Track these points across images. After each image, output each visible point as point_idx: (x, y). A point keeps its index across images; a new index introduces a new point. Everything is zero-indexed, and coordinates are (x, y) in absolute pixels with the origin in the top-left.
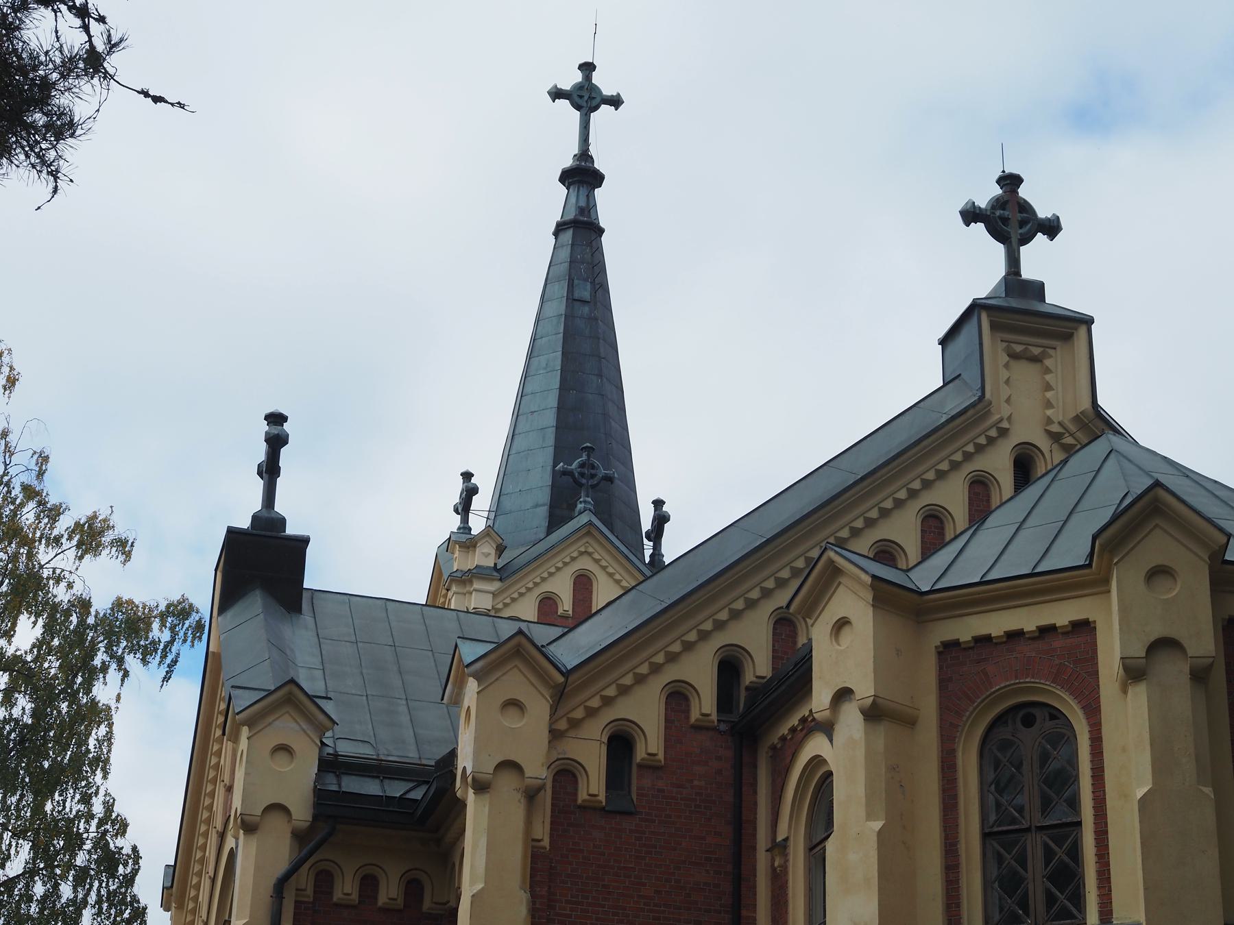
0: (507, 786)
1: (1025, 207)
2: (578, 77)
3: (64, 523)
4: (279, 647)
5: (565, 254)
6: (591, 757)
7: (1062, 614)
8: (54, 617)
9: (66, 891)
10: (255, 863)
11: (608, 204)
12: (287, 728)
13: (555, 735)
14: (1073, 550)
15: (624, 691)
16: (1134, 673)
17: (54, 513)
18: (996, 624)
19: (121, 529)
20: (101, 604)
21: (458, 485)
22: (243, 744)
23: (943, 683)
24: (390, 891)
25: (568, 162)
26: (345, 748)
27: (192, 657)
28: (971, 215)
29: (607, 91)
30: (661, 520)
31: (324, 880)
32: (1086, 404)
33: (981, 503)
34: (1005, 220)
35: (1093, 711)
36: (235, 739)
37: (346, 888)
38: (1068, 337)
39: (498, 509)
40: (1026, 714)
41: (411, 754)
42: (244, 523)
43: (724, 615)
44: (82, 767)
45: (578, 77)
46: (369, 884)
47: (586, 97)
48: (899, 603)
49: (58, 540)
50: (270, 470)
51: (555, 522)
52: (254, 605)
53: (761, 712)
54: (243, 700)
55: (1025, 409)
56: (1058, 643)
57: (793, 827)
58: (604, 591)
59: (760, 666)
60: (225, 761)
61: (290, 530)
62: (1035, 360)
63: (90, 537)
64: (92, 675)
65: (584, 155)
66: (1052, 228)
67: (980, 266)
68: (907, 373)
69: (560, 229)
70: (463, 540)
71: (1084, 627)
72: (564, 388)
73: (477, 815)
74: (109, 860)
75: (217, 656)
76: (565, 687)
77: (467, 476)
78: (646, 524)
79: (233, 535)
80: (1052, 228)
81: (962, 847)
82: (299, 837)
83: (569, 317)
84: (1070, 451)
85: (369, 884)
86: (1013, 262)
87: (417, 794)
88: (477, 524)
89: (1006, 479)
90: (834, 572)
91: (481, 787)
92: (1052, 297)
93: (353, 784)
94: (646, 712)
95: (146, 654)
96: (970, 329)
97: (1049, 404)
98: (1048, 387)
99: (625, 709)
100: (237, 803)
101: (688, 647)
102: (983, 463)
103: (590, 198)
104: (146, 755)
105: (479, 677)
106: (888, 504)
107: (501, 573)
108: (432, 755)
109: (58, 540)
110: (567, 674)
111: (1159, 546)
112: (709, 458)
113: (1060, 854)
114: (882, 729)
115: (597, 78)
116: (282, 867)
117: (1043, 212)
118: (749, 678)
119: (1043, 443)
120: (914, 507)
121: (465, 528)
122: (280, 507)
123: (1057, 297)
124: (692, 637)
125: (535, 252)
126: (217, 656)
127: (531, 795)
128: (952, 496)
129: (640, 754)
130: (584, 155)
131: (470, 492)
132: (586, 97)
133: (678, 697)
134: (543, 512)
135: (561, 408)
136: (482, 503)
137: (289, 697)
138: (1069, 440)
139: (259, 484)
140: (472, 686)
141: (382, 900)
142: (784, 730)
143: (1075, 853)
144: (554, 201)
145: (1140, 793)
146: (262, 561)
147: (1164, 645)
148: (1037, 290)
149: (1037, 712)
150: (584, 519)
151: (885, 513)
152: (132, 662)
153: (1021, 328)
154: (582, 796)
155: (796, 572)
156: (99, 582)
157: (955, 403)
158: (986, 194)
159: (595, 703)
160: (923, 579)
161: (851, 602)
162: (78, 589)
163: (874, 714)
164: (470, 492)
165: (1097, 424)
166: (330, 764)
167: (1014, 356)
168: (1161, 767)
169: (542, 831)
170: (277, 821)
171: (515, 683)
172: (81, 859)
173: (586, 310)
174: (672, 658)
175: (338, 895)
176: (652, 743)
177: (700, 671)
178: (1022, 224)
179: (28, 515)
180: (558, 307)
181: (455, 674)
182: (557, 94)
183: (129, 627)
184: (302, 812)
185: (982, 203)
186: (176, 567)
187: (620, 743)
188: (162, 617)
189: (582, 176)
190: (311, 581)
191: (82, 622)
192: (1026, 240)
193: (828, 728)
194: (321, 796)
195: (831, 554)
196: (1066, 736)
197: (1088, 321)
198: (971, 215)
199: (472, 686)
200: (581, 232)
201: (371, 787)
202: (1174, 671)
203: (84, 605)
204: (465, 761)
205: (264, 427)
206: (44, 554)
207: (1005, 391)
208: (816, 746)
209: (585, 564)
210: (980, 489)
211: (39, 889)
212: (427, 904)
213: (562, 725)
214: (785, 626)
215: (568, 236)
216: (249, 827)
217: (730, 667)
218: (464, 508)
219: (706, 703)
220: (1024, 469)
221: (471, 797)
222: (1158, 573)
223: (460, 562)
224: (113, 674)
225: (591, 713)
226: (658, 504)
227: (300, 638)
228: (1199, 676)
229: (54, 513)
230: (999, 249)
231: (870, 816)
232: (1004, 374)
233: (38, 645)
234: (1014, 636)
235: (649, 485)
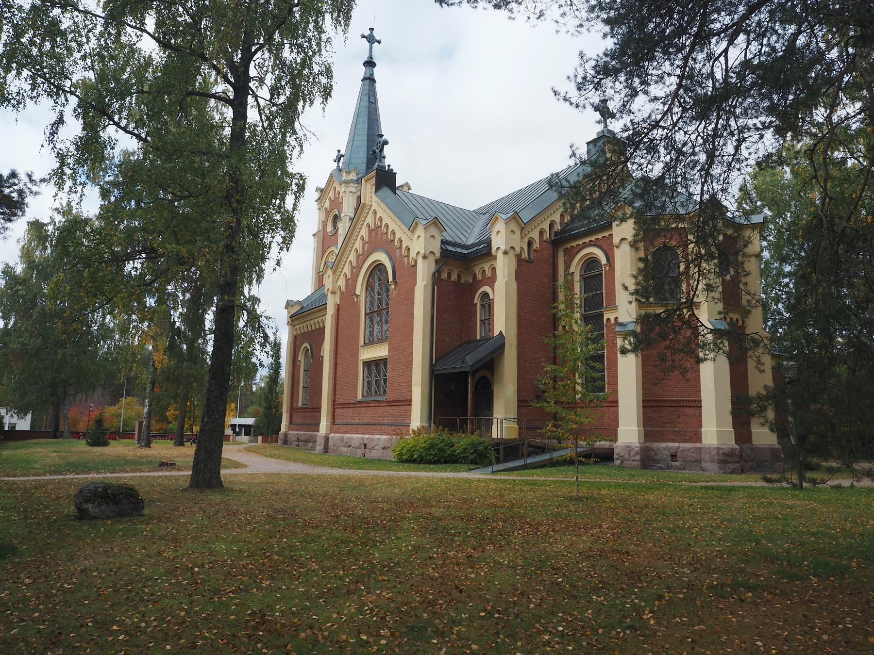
2: (369, 32)
11: (377, 72)
24: (454, 277)
29: (377, 38)
37: (444, 276)
40: (666, 248)
45: (369, 32)
46: (449, 274)
47: (371, 39)
65: (371, 57)
69: (364, 80)
72: (369, 129)
82: (437, 261)
83: (369, 107)
85: (449, 274)
99: (531, 235)
115: (374, 33)
121: (338, 166)
132: (371, 39)
133: (541, 233)
134: (365, 165)
135: (368, 135)
141: (453, 279)
142: (574, 244)
144: (362, 71)
166: (443, 242)
175: (443, 277)
177: (546, 226)
182: (363, 36)
184: (438, 255)
189: (370, 64)
200: (370, 80)
201: (459, 250)
212: (462, 281)
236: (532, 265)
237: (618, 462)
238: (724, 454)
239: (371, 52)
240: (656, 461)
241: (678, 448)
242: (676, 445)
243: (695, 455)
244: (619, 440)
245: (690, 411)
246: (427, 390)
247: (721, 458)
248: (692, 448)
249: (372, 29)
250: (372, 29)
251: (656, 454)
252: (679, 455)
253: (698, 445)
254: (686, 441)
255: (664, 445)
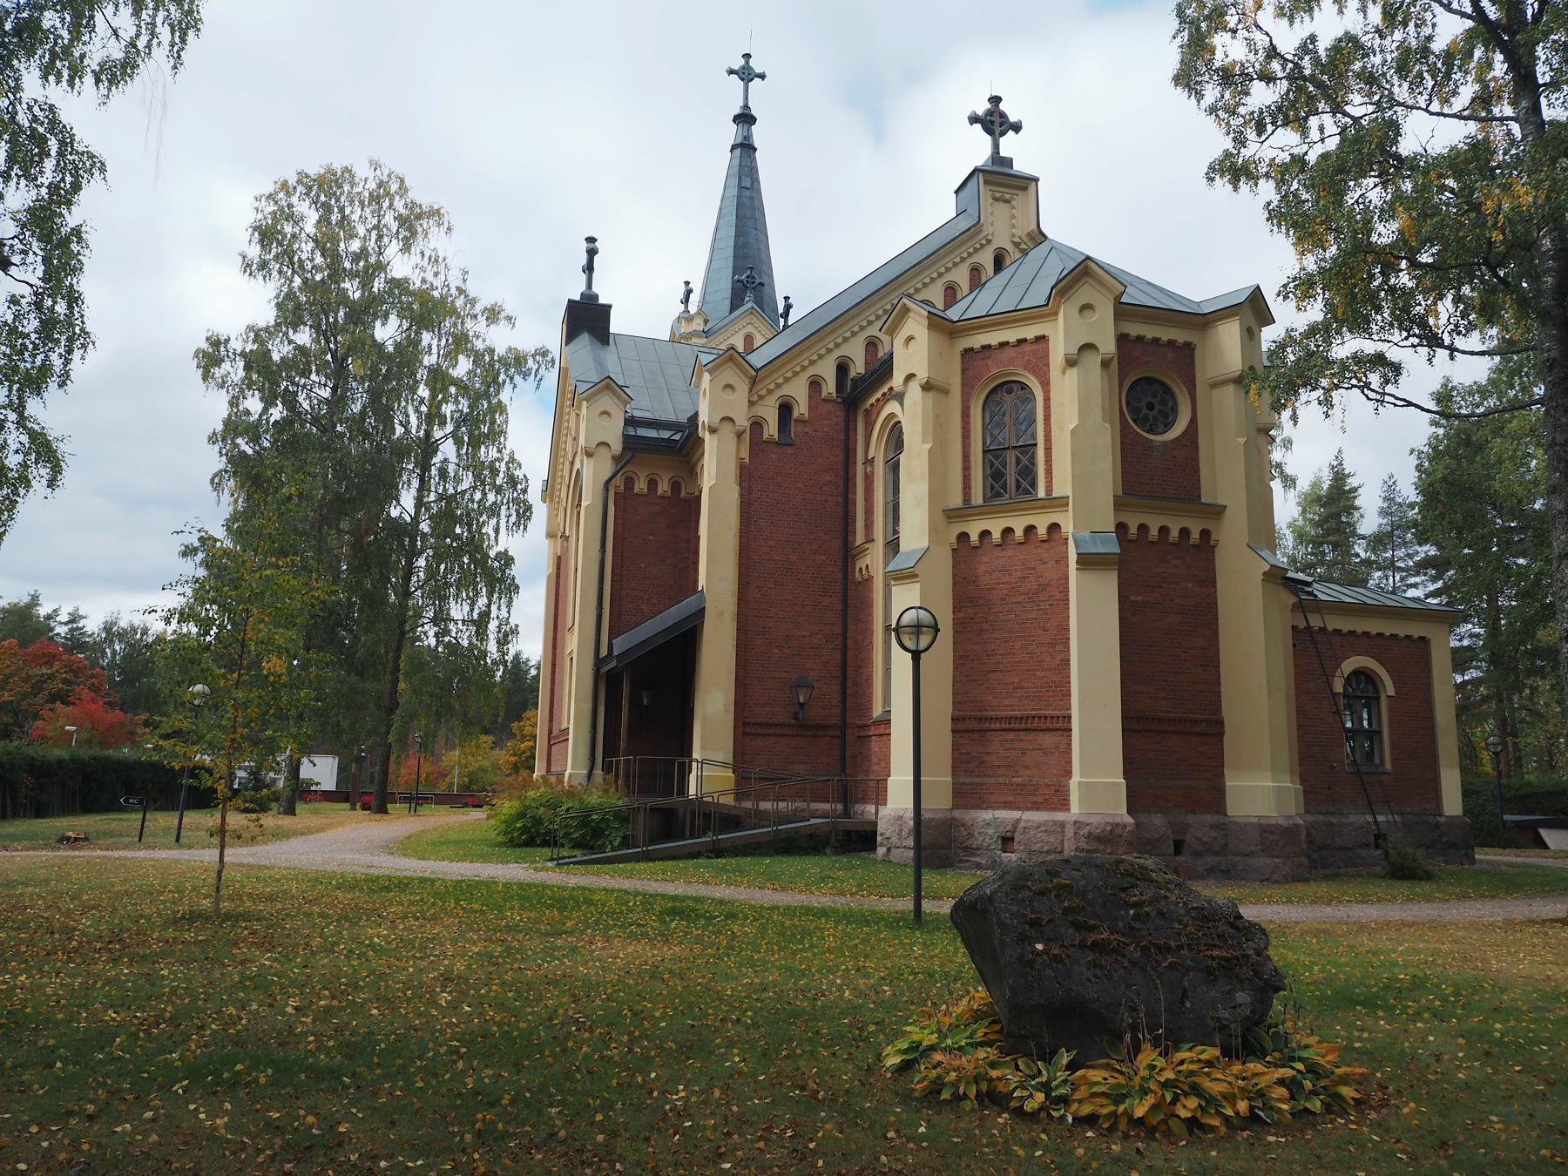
0: (727, 429)
1: (1003, 115)
2: (742, 62)
3: (479, 307)
4: (600, 363)
5: (736, 162)
6: (771, 416)
7: (1030, 332)
8: (477, 357)
9: (491, 497)
10: (593, 473)
12: (607, 402)
13: (751, 403)
14: (1038, 296)
15: (787, 380)
16: (1071, 363)
17: (473, 302)
18: (993, 338)
19: (508, 311)
20: (500, 350)
21: (683, 288)
22: (584, 411)
23: (964, 370)
24: (663, 487)
25: (737, 111)
26: (637, 414)
27: (551, 377)
28: (974, 119)
30: (788, 307)
31: (629, 482)
32: (1034, 226)
33: (976, 281)
34: (992, 123)
35: (1046, 385)
36: (579, 408)
37: (641, 486)
38: (1025, 189)
39: (703, 301)
40: (1007, 386)
41: (672, 417)
42: (577, 298)
43: (840, 340)
44: (495, 435)
46: (653, 484)
47: (746, 74)
48: (940, 325)
49: (475, 316)
50: (589, 268)
51: (733, 308)
52: (584, 340)
53: (861, 389)
54: (582, 387)
55: (1001, 228)
56: (1027, 348)
57: (878, 451)
58: (759, 340)
59: (858, 368)
60: (572, 424)
61: (602, 301)
62: (1007, 201)
63: (493, 314)
64: (500, 387)
65: (746, 107)
66: (1017, 128)
67: (978, 149)
68: (932, 209)
69: (733, 148)
70: (686, 317)
71: (1042, 339)
73: (710, 443)
74: (513, 481)
75: (567, 370)
76: (756, 378)
77: (687, 283)
78: (781, 310)
79: (571, 304)
80: (1017, 128)
81: (972, 458)
82: (616, 459)
83: (739, 197)
84: (1025, 253)
85: (653, 484)
86: (996, 146)
87: (677, 437)
88: (693, 309)
89: (965, 286)
90: (906, 310)
91: (713, 431)
92: (1016, 167)
93: (642, 432)
94: (798, 391)
95: (525, 376)
96: (973, 184)
97: (1014, 226)
98: (1014, 217)
100: (582, 442)
101: (821, 357)
102: (976, 259)
103: (749, 130)
104: (527, 435)
105: (710, 372)
106: (927, 280)
107: (707, 334)
108: (683, 418)
109: (475, 316)
110: (757, 371)
111: (1086, 293)
112: (814, 268)
113: (1024, 460)
114: (930, 395)
116: (608, 475)
117: (1013, 119)
118: (853, 374)
119: (1010, 248)
120: (862, 336)
122: (595, 289)
123: (1020, 167)
124: (823, 351)
125: (720, 161)
126: (567, 370)
127: (739, 435)
128: (961, 276)
129: (796, 414)
130: (746, 107)
131: (689, 292)
132: (746, 74)
133: (815, 384)
134: (728, 302)
136: (695, 298)
137: (608, 385)
138: (1023, 246)
139: (584, 277)
140: (706, 376)
141: (660, 492)
142: (873, 400)
143: (1033, 460)
144: (731, 133)
145: (1072, 427)
146: (587, 318)
147: (1088, 347)
148: (1009, 162)
149: (1015, 387)
150: (750, 305)
151: (925, 285)
152: (517, 379)
153: (1000, 181)
154: (766, 436)
155: (885, 311)
156: (499, 339)
157: (964, 224)
158: (982, 107)
159: (772, 386)
160: (954, 314)
161: (916, 326)
162: (488, 343)
163: (927, 387)
164: (689, 292)
165: (1039, 237)
166: (630, 422)
167: (996, 199)
168: (1083, 413)
169: (745, 454)
170: (603, 450)
171: (730, 375)
172: (499, 481)
173: (748, 193)
174: (812, 363)
175: (637, 490)
176: (801, 408)
177: (827, 371)
178: (1001, 124)
179: (459, 303)
180: (734, 191)
181: (697, 370)
183: (517, 362)
184: (617, 447)
185: (980, 112)
186: (537, 328)
187: (785, 409)
188: (533, 356)
189: (745, 118)
190: (614, 328)
191: (492, 359)
192: (1003, 134)
193: (900, 397)
194: (626, 438)
195: (905, 300)
196: (1031, 398)
197: (1036, 180)
198: (974, 119)
199: (706, 376)
200: (745, 148)
201: (652, 433)
202: (1093, 361)
203: (491, 351)
204: (704, 418)
205: (585, 244)
206: (469, 324)
207: (991, 219)
208: (892, 407)
209: (750, 329)
210: (976, 271)
211: (478, 496)
212: (683, 494)
213: (755, 398)
214: (872, 345)
215: (738, 152)
216: (589, 455)
217: (842, 368)
218: (686, 300)
219: (830, 388)
220: (999, 264)
221: (707, 436)
222: (1086, 308)
223: (685, 328)
224: (508, 387)
225: (770, 392)
226: (787, 298)
227: (610, 356)
228: (1105, 364)
229: (473, 302)
230: (988, 138)
231: (924, 442)
232: (990, 209)
233: (469, 373)
234: (1003, 345)
235: (781, 290)
236: (790, 450)
237: (881, 851)
238: (1089, 836)
239: (746, 98)
240: (971, 850)
241: (1018, 821)
242: (1016, 814)
243: (1051, 839)
244: (889, 805)
245: (1048, 740)
246: (587, 706)
247: (1083, 845)
248: (1045, 823)
249: (747, 56)
250: (747, 56)
251: (971, 835)
252: (1017, 837)
253: (1060, 816)
254: (1036, 807)
255: (987, 815)
